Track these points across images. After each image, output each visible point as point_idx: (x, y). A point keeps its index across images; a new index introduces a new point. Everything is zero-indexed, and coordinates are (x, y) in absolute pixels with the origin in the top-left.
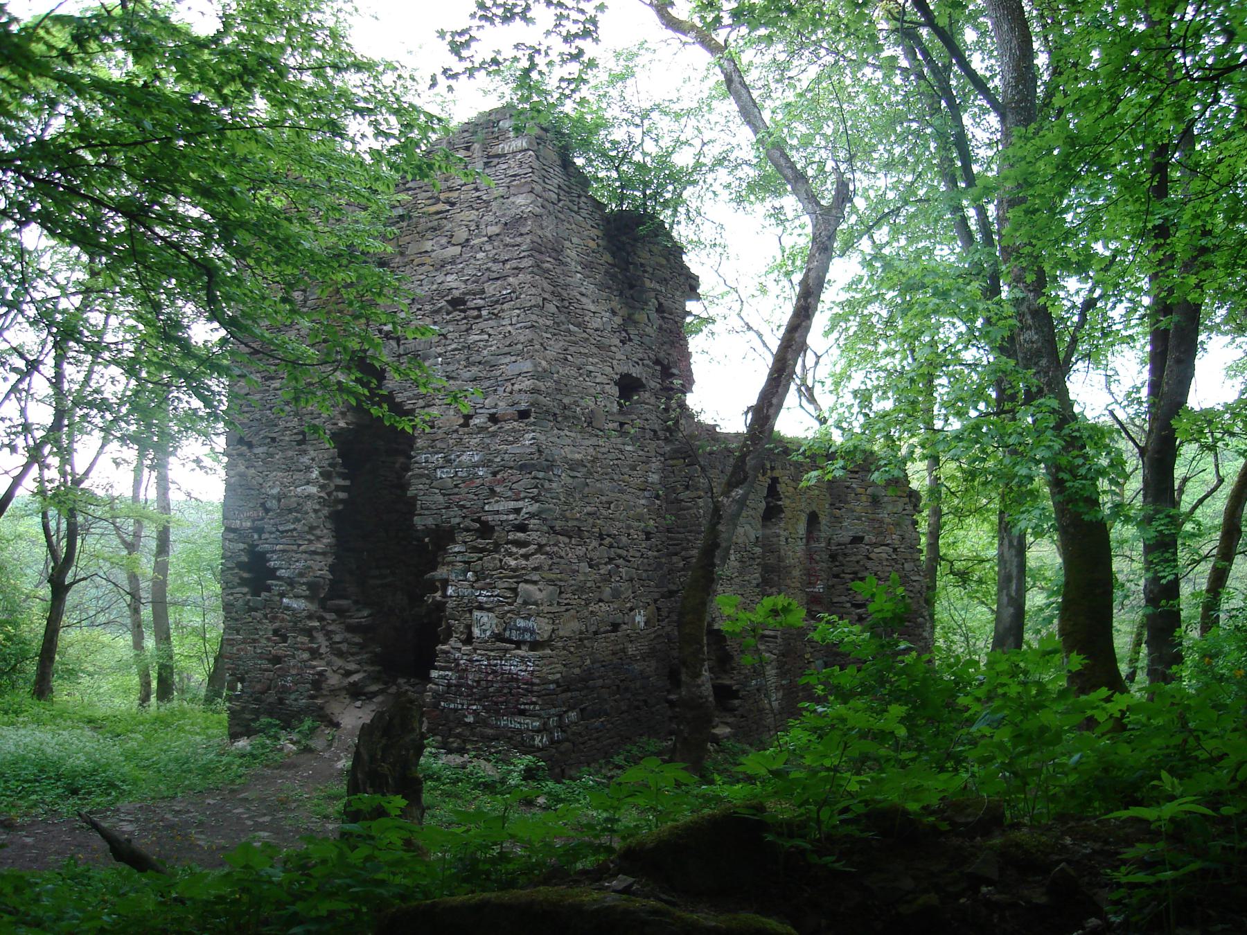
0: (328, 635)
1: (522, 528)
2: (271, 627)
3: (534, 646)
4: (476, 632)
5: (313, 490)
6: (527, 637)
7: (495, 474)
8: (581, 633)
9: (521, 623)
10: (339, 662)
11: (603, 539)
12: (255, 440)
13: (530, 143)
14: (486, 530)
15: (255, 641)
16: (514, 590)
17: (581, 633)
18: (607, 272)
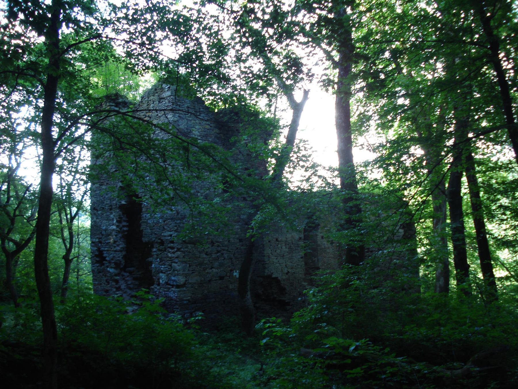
0: (126, 281)
1: (172, 242)
2: (105, 279)
3: (178, 286)
4: (161, 281)
5: (114, 227)
6: (175, 283)
7: (164, 221)
8: (201, 281)
9: (173, 278)
10: (129, 291)
11: (214, 244)
12: (98, 208)
13: (172, 93)
14: (162, 243)
15: (101, 284)
16: (171, 265)
17: (201, 281)
18: (215, 137)
